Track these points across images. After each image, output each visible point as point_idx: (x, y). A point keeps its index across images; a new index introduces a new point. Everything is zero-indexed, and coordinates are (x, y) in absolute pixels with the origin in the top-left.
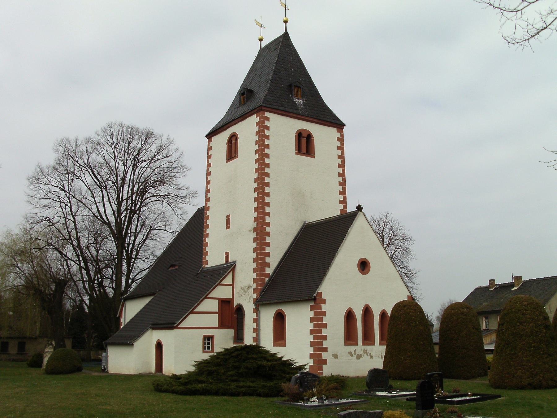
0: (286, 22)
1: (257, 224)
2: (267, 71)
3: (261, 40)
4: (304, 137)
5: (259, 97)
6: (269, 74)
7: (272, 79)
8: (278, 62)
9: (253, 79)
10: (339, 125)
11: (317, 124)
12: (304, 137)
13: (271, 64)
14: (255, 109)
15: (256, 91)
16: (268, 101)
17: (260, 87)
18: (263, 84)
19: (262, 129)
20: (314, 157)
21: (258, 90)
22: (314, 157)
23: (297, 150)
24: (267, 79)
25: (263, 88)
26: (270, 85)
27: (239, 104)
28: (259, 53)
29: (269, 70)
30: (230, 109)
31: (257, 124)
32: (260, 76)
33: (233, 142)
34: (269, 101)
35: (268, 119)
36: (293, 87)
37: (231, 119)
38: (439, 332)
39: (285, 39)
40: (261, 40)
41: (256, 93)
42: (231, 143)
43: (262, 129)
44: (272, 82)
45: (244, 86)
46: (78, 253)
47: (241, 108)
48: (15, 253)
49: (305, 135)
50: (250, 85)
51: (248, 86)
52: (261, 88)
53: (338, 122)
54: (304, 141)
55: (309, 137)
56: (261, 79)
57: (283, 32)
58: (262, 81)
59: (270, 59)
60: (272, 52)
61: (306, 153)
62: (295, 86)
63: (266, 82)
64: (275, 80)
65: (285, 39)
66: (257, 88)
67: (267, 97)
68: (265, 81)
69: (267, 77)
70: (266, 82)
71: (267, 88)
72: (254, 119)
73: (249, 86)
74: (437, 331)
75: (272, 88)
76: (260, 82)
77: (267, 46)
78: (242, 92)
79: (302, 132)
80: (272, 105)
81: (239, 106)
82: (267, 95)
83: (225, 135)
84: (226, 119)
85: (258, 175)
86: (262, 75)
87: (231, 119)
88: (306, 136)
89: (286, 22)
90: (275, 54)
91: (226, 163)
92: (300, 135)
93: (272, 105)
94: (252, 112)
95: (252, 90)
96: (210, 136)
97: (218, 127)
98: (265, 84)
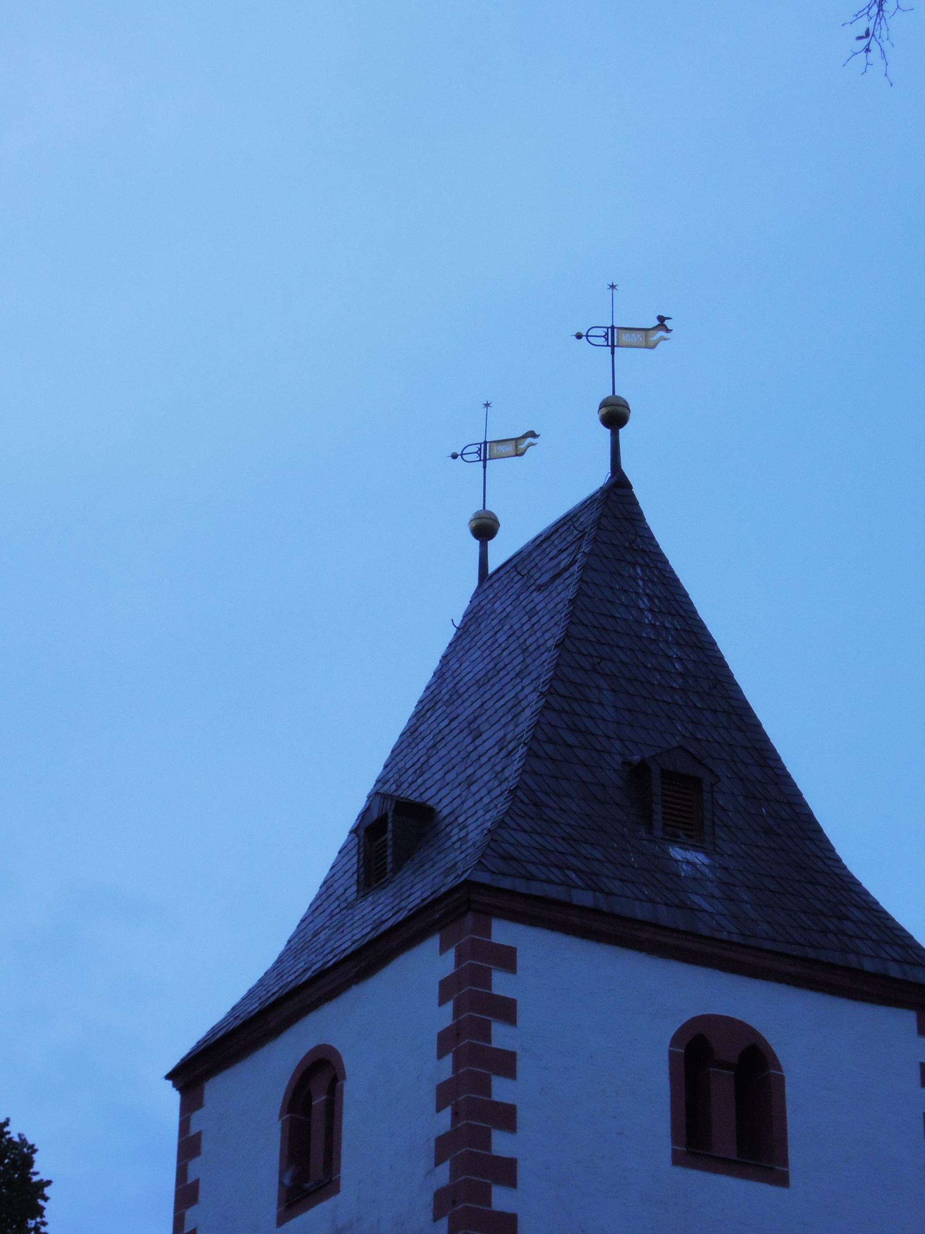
1: (456, 1115)
2: (512, 694)
5: (459, 839)
6: (519, 709)
7: (534, 738)
8: (567, 643)
9: (434, 746)
11: (722, 974)
13: (535, 655)
14: (436, 901)
15: (445, 812)
16: (507, 858)
17: (470, 785)
18: (489, 766)
20: (782, 1180)
21: (456, 803)
22: (782, 1180)
24: (509, 737)
25: (484, 791)
26: (524, 770)
27: (354, 888)
28: (476, 602)
29: (519, 687)
30: (308, 921)
31: (447, 989)
32: (474, 726)
33: (319, 1100)
34: (513, 858)
37: (306, 970)
38: (355, 885)
41: (447, 821)
42: (306, 1108)
44: (531, 753)
45: (390, 788)
47: (366, 906)
50: (420, 781)
51: (411, 784)
52: (474, 788)
56: (478, 742)
57: (600, 476)
58: (481, 750)
59: (525, 628)
60: (539, 588)
61: (734, 1157)
63: (502, 754)
64: (550, 741)
66: (457, 792)
67: (502, 832)
68: (496, 750)
69: (511, 727)
70: (502, 754)
71: (504, 786)
73: (414, 787)
74: (354, 884)
75: (534, 787)
76: (474, 756)
77: (515, 564)
80: (531, 878)
81: (356, 899)
82: (503, 821)
84: (280, 975)
85: (456, 1068)
86: (479, 721)
87: (306, 970)
90: (557, 600)
91: (282, 1219)
93: (531, 878)
95: (430, 803)
97: (238, 1022)
98: (499, 768)
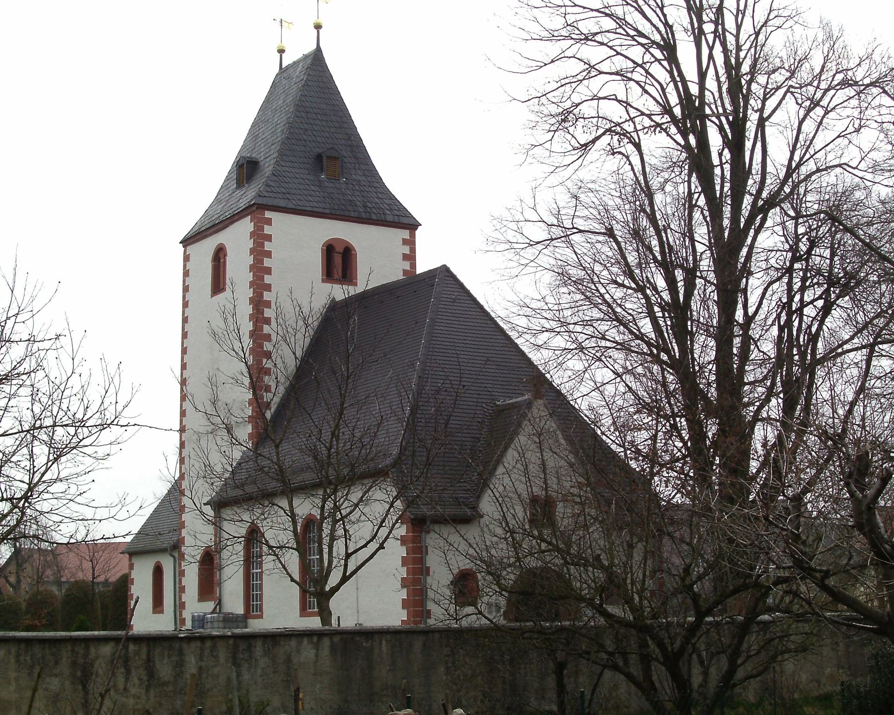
0: (318, 27)
3: (281, 51)
4: (338, 253)
10: (412, 225)
12: (338, 253)
19: (260, 238)
23: (325, 275)
35: (269, 222)
36: (325, 159)
39: (316, 60)
40: (281, 51)
43: (260, 238)
46: (643, 282)
48: (496, 603)
49: (340, 248)
53: (405, 220)
54: (338, 260)
55: (348, 253)
62: (327, 157)
65: (316, 60)
72: (246, 225)
78: (240, 163)
79: (334, 244)
83: (208, 246)
88: (342, 250)
89: (318, 27)
92: (329, 249)
94: (243, 214)
96: (187, 242)
